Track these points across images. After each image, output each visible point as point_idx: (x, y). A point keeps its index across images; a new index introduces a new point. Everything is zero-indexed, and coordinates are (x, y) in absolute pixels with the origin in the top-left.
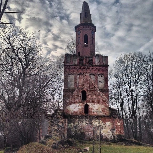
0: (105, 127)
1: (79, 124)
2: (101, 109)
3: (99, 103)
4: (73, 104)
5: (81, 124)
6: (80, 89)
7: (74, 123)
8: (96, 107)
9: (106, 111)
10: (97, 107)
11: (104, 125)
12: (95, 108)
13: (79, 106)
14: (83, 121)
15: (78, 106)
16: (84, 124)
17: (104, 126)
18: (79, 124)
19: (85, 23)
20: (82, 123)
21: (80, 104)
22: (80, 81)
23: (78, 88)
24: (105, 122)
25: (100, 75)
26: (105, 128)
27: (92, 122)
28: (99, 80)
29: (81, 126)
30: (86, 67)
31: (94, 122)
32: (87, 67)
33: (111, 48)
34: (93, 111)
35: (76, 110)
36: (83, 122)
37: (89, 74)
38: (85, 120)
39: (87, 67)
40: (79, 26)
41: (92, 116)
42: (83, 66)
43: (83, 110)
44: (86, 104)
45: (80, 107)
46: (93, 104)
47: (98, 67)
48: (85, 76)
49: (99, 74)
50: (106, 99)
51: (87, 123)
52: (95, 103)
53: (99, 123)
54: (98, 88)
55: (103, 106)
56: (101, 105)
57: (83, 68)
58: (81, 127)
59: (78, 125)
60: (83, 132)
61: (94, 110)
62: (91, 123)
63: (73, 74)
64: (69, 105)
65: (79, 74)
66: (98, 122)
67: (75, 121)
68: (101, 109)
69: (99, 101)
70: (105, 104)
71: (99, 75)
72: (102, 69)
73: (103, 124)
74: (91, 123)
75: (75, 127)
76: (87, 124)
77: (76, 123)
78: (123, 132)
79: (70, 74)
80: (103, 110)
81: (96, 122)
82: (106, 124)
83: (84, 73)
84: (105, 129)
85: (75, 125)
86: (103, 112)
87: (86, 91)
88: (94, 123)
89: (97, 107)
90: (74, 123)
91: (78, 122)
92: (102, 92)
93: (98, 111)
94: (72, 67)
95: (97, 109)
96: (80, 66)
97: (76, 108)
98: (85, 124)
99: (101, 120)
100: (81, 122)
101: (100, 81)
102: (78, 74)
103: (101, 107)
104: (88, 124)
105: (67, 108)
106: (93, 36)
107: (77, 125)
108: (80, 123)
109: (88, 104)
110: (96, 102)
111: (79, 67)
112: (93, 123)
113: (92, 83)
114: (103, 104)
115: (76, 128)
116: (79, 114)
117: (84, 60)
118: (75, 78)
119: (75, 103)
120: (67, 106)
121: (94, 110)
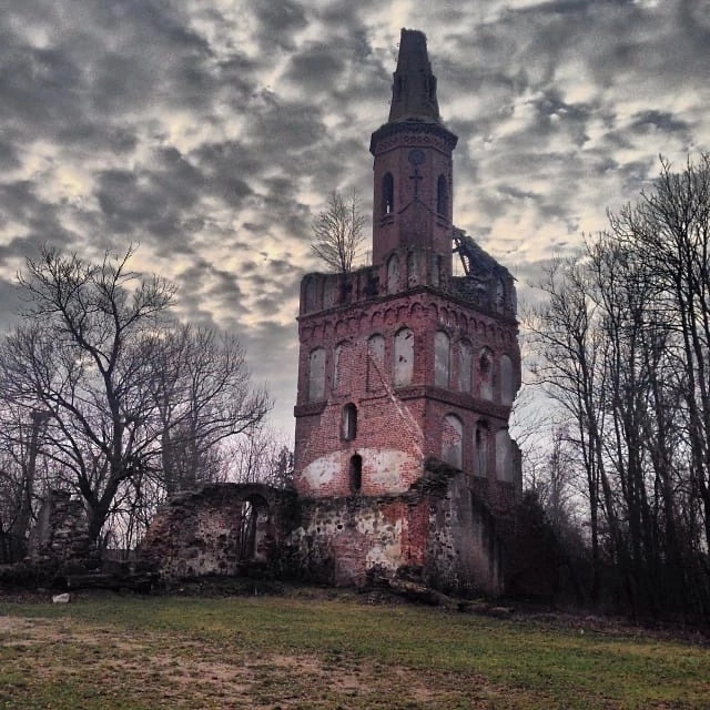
1: (319, 529)
2: (397, 469)
3: (393, 446)
5: (325, 529)
6: (340, 400)
7: (306, 529)
9: (147, 388)
10: (385, 460)
11: (389, 529)
15: (331, 464)
16: (332, 527)
17: (390, 534)
18: (319, 529)
20: (327, 525)
21: (338, 454)
22: (344, 370)
23: (333, 396)
24: (391, 517)
26: (391, 543)
28: (398, 354)
32: (360, 310)
33: (538, 225)
34: (373, 477)
35: (327, 478)
37: (366, 338)
38: (338, 515)
41: (367, 497)
45: (338, 468)
46: (376, 451)
47: (393, 302)
49: (396, 329)
52: (380, 446)
53: (375, 524)
54: (393, 385)
55: (405, 455)
57: (349, 319)
59: (317, 534)
60: (330, 559)
61: (376, 476)
66: (373, 520)
67: (309, 519)
68: (397, 469)
69: (392, 438)
74: (352, 526)
75: (309, 539)
76: (340, 527)
77: (312, 528)
79: (316, 349)
81: (367, 519)
84: (392, 547)
85: (310, 534)
87: (357, 405)
90: (306, 529)
91: (318, 523)
92: (403, 400)
93: (389, 479)
94: (319, 321)
96: (340, 314)
97: (325, 473)
99: (381, 513)
101: (401, 359)
102: (338, 345)
103: (399, 459)
105: (304, 475)
106: (416, 171)
107: (314, 532)
108: (322, 524)
109: (361, 452)
110: (383, 444)
112: (357, 523)
113: (377, 370)
115: (310, 546)
116: (335, 493)
117: (413, 292)
118: (327, 362)
119: (324, 453)
120: (303, 467)
121: (376, 476)
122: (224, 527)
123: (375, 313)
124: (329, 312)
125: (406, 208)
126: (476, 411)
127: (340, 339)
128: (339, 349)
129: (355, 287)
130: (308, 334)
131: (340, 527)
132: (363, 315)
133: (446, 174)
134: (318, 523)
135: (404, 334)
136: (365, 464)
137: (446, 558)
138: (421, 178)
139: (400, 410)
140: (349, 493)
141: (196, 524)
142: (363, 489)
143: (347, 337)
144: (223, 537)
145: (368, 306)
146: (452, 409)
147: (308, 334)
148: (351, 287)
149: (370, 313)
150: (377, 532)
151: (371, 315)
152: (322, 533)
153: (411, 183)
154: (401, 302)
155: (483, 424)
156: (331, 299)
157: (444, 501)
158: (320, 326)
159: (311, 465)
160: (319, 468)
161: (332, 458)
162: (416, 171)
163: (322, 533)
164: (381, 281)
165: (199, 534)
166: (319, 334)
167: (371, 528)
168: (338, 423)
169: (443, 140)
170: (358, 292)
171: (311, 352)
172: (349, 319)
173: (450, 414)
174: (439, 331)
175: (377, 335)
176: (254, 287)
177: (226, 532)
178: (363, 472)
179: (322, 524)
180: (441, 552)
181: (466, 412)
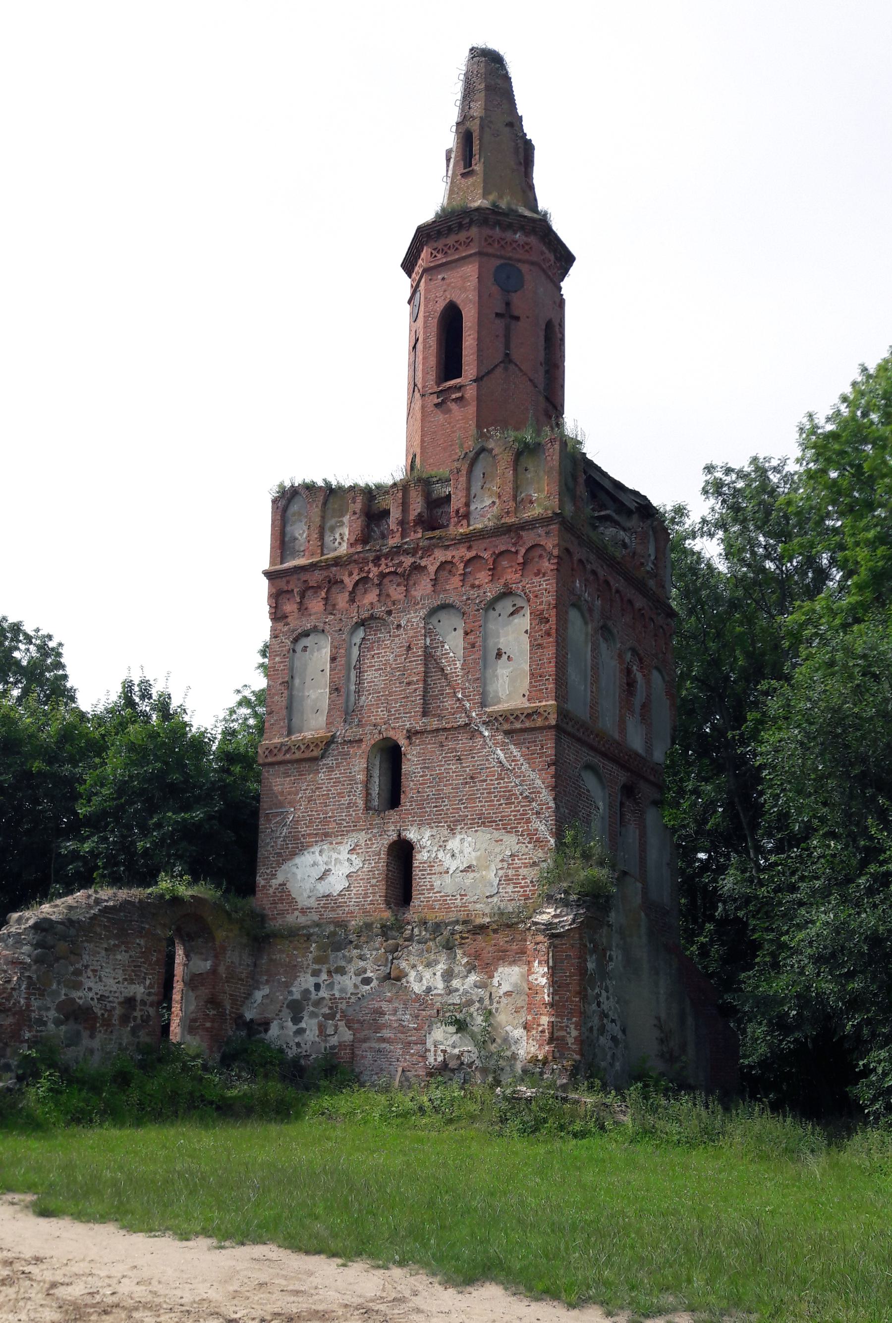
0: (487, 1002)
1: (317, 987)
3: (484, 821)
4: (316, 849)
5: (331, 986)
8: (461, 852)
10: (467, 850)
11: (482, 985)
12: (453, 865)
13: (353, 857)
14: (343, 964)
18: (317, 987)
19: (495, 210)
20: (337, 978)
22: (369, 676)
25: (499, 607)
27: (404, 965)
29: (333, 998)
30: (401, 563)
31: (414, 967)
32: (408, 561)
35: (336, 883)
36: (341, 971)
39: (412, 560)
40: (417, 249)
42: (386, 556)
43: (374, 881)
44: (399, 835)
48: (399, 626)
50: (531, 786)
51: (369, 974)
53: (448, 975)
55: (511, 843)
56: (497, 835)
58: (331, 1008)
59: (313, 996)
62: (398, 979)
63: (321, 626)
64: (293, 854)
65: (362, 623)
66: (441, 967)
70: (528, 821)
71: (491, 605)
72: (517, 552)
73: (473, 978)
74: (394, 978)
76: (367, 981)
78: (570, 1040)
79: (306, 634)
80: (511, 872)
82: (495, 981)
83: (389, 613)
86: (510, 889)
88: (412, 975)
89: (467, 850)
91: (316, 973)
92: (507, 733)
95: (469, 868)
98: (356, 986)
100: (329, 973)
104: (374, 983)
105: (280, 878)
106: (508, 304)
108: (324, 976)
109: (411, 835)
110: (463, 819)
111: (361, 570)
114: (508, 829)
120: (279, 865)
122: (132, 982)
123: (443, 564)
124: (337, 562)
125: (489, 373)
126: (623, 766)
127: (365, 615)
128: (361, 633)
129: (395, 514)
130: (290, 607)
131: (367, 981)
132: (417, 568)
133: (556, 324)
134: (316, 973)
135: (507, 606)
136: (421, 857)
137: (610, 1044)
138: (517, 318)
139: (500, 752)
140: (387, 915)
141: (78, 973)
142: (417, 901)
143: (380, 610)
144: (130, 1002)
145: (427, 551)
146: (596, 760)
147: (290, 607)
148: (386, 513)
149: (431, 564)
150: (450, 991)
151: (432, 569)
152: (323, 993)
153: (500, 324)
154: (502, 544)
155: (629, 791)
156: (342, 539)
157: (605, 930)
158: (317, 588)
159: (298, 860)
160: (315, 864)
161: (344, 849)
162: (508, 304)
163: (323, 993)
164: (457, 502)
165: (80, 996)
166: (316, 605)
167: (440, 985)
168: (361, 777)
169: (552, 258)
170: (402, 523)
171: (296, 640)
172: (382, 576)
173: (588, 767)
174: (574, 605)
175: (444, 607)
176: (62, 660)
177: (139, 990)
178: (416, 872)
179: (324, 976)
180: (602, 1030)
181: (610, 765)
